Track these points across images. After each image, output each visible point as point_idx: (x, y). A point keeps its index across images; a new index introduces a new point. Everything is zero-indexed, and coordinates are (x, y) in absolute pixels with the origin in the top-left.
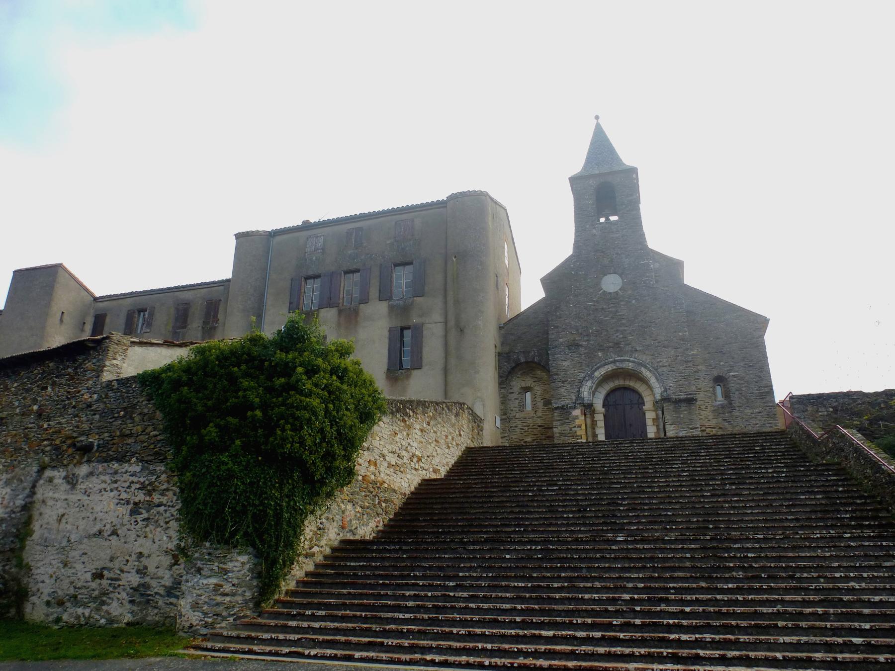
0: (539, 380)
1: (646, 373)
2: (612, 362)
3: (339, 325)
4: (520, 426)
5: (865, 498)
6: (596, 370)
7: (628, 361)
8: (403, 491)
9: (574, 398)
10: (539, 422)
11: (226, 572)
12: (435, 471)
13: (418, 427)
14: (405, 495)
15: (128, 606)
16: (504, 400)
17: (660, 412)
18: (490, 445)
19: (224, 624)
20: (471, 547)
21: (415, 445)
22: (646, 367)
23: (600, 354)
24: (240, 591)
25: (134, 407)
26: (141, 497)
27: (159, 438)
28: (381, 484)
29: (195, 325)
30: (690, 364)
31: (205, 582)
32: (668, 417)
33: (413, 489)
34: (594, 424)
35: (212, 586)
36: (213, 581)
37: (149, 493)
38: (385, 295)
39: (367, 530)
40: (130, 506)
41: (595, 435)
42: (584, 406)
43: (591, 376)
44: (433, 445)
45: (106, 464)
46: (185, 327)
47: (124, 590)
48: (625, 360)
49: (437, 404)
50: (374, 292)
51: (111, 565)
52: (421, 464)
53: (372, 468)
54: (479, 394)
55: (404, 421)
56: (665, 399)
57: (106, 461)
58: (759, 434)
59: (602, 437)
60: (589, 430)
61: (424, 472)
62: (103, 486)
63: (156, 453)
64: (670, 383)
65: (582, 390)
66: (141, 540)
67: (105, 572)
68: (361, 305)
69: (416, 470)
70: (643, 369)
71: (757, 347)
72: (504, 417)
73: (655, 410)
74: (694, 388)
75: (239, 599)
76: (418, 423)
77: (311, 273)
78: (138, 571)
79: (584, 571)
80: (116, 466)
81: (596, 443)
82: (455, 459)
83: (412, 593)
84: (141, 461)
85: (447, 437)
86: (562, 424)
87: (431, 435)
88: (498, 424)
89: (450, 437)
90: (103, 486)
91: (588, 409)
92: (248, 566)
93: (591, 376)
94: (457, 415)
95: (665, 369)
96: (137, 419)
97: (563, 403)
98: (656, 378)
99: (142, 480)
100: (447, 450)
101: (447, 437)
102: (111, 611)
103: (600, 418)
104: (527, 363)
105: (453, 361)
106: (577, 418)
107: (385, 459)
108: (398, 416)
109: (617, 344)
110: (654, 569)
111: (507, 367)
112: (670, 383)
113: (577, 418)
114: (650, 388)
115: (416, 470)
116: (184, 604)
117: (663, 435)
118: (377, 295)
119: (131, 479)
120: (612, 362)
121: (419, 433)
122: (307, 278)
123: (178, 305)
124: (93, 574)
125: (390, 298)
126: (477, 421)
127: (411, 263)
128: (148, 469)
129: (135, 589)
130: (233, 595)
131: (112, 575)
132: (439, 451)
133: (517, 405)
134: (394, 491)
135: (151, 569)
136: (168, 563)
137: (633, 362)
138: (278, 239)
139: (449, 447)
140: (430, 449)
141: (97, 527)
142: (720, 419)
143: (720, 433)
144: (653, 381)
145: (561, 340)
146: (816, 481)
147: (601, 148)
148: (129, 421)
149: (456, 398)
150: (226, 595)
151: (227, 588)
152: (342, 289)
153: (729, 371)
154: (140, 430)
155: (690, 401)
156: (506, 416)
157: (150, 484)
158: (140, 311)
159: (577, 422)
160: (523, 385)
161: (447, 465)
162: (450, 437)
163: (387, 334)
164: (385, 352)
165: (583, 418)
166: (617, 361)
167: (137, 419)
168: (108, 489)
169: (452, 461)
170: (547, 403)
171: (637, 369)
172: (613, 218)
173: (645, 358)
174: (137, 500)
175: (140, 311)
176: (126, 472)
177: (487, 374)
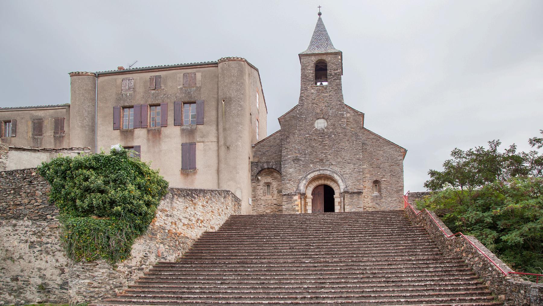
0: (276, 178)
1: (336, 177)
2: (318, 170)
3: (148, 140)
4: (263, 204)
5: (429, 242)
6: (309, 174)
7: (327, 170)
8: (193, 238)
9: (295, 189)
10: (275, 202)
11: (94, 277)
12: (212, 228)
13: (201, 204)
14: (194, 240)
15: (38, 294)
16: (254, 189)
17: (342, 199)
18: (245, 214)
19: (96, 301)
20: (230, 266)
21: (199, 214)
22: (337, 174)
23: (311, 166)
24: (103, 286)
25: (20, 188)
26: (34, 238)
27: (40, 207)
28: (180, 234)
29: (48, 133)
30: (361, 173)
31: (83, 281)
32: (346, 201)
33: (199, 237)
34: (306, 204)
36: (87, 281)
37: (40, 237)
38: (178, 122)
39: (172, 258)
40: (28, 244)
41: (306, 210)
43: (305, 178)
44: (210, 214)
45: (7, 221)
46: (41, 135)
47: (33, 286)
48: (325, 170)
49: (212, 191)
50: (171, 120)
51: (22, 274)
52: (203, 224)
53: (174, 226)
54: (239, 186)
55: (192, 201)
56: (346, 192)
57: (7, 219)
58: (391, 212)
59: (310, 211)
60: (303, 207)
61: (205, 228)
62: (8, 232)
63: (40, 215)
64: (349, 183)
65: (300, 185)
66: (38, 262)
67: (19, 277)
68: (163, 128)
69: (200, 227)
70: (335, 175)
72: (254, 199)
73: (340, 198)
74: (362, 186)
75: (103, 289)
76: (200, 202)
77: (126, 104)
78: (40, 277)
79: (287, 276)
80: (14, 222)
81: (306, 214)
82: (224, 221)
83: (198, 286)
84: (31, 219)
85: (218, 209)
86: (288, 204)
87: (209, 208)
88: (251, 202)
89: (221, 210)
90: (8, 232)
91: (303, 196)
92: (106, 274)
93: (305, 178)
94: (225, 197)
95: (347, 175)
96: (24, 195)
97: (288, 192)
99: (34, 230)
100: (219, 217)
101: (218, 209)
102: (27, 297)
103: (309, 201)
104: (268, 168)
105: (222, 166)
106: (296, 200)
107: (181, 221)
108: (188, 198)
109: (322, 160)
110: (321, 274)
111: (256, 170)
112: (349, 183)
113: (296, 200)
114: (338, 185)
115: (200, 227)
116: (72, 292)
117: (343, 211)
118: (173, 122)
119: (26, 229)
120: (318, 170)
121: (202, 207)
122: (124, 108)
123: (34, 120)
124: (11, 279)
125: (181, 125)
126: (237, 201)
127: (195, 103)
128: (36, 224)
129: (39, 286)
130: (100, 288)
131: (23, 279)
132: (214, 217)
133: (262, 192)
134: (188, 238)
135: (48, 275)
136: (58, 273)
137: (330, 171)
138: (101, 79)
139: (220, 215)
140: (209, 216)
141: (35, 250)
142: (374, 203)
143: (374, 210)
144: (340, 182)
145: (289, 156)
146: (410, 235)
147: (320, 33)
148: (18, 196)
149: (225, 187)
150: (96, 287)
151: (95, 284)
152: (149, 116)
153: (382, 178)
154: (27, 202)
155: (359, 193)
156: (255, 198)
157: (39, 232)
158: (6, 122)
159: (296, 203)
160: (266, 181)
161: (219, 224)
162: (221, 210)
163: (180, 147)
164: (180, 158)
165: (300, 200)
166: (321, 170)
167: (24, 195)
168: (12, 234)
169: (222, 222)
170: (280, 192)
172: (325, 84)
173: (337, 169)
174: (32, 240)
175: (6, 122)
176: (22, 225)
177: (244, 174)
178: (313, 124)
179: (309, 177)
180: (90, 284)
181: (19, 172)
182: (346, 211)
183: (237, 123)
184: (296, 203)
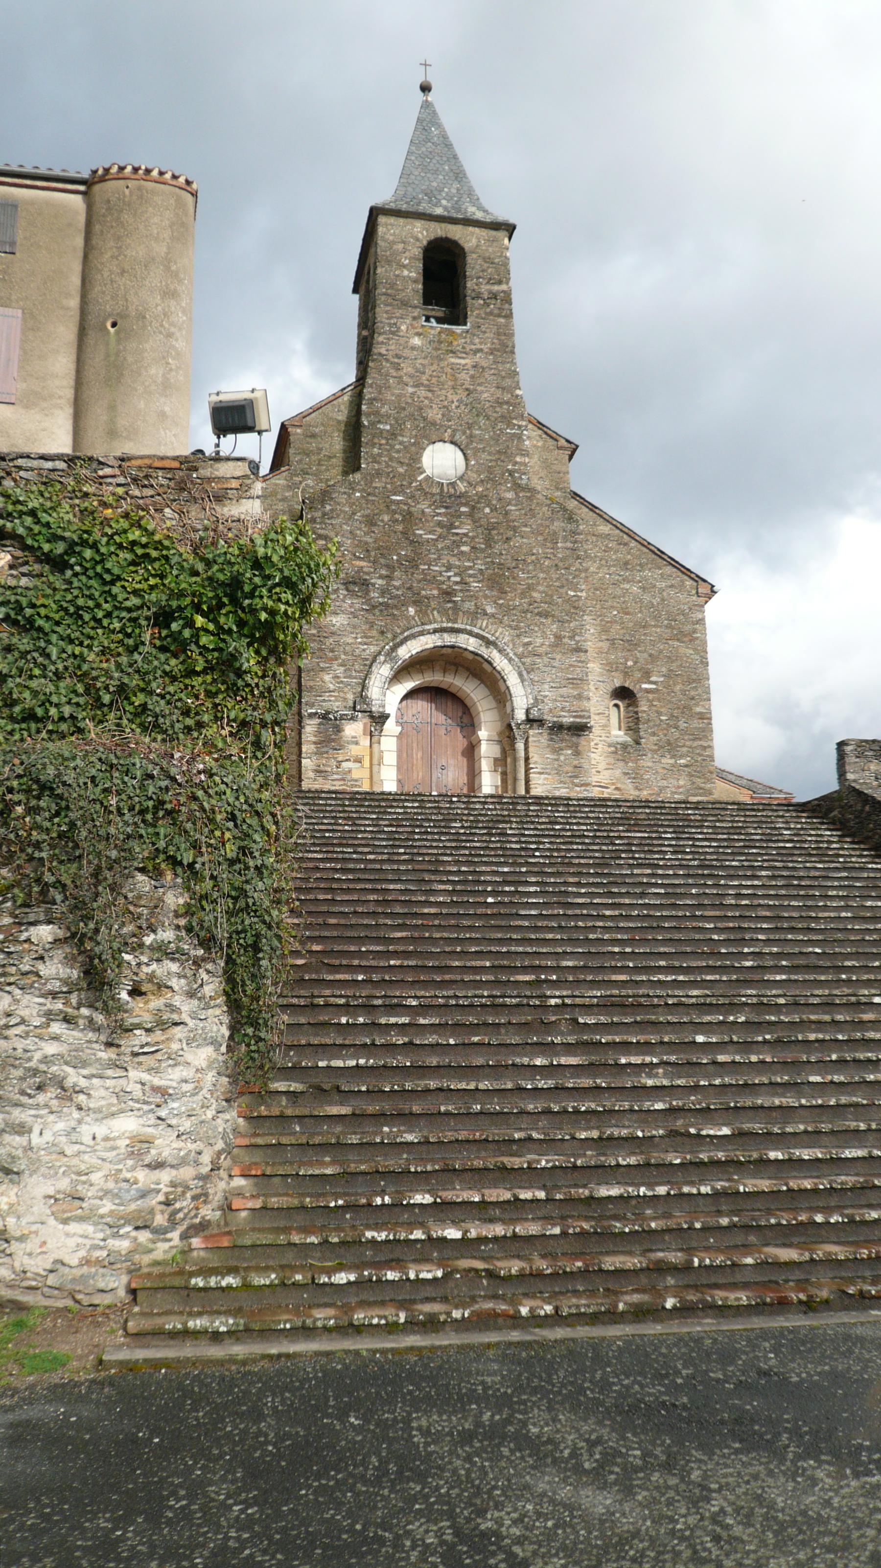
1: (500, 662)
2: (435, 631)
6: (402, 643)
7: (470, 633)
9: (350, 697)
22: (501, 651)
23: (412, 611)
31: (101, 1130)
35: (123, 1143)
36: (128, 1125)
42: (372, 717)
43: (391, 654)
71: (693, 640)
98: (520, 675)
109: (448, 594)
142: (618, 773)
144: (513, 680)
153: (640, 681)
159: (354, 750)
171: (484, 651)
178: (416, 459)
179: (405, 652)
180: (140, 1146)
181: (161, 479)
182: (534, 792)
183: (162, 415)
184: (354, 750)
